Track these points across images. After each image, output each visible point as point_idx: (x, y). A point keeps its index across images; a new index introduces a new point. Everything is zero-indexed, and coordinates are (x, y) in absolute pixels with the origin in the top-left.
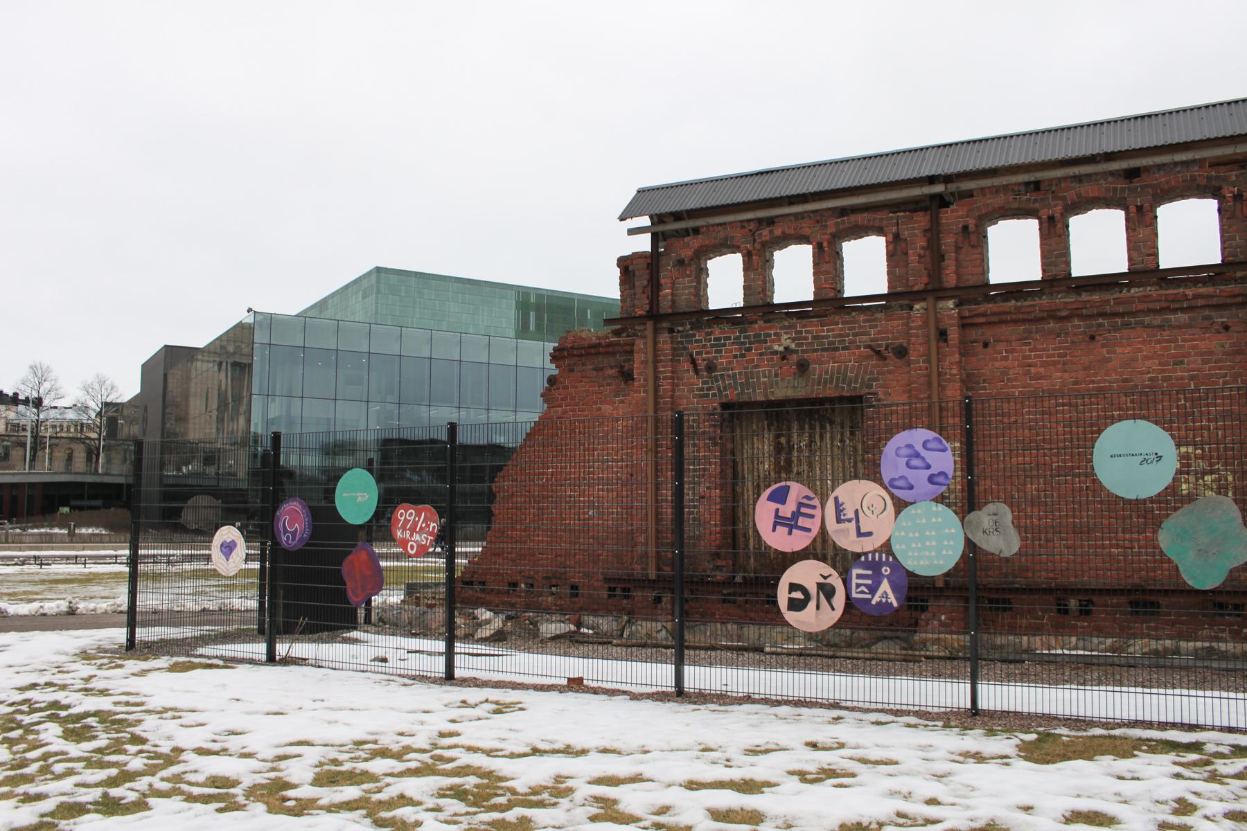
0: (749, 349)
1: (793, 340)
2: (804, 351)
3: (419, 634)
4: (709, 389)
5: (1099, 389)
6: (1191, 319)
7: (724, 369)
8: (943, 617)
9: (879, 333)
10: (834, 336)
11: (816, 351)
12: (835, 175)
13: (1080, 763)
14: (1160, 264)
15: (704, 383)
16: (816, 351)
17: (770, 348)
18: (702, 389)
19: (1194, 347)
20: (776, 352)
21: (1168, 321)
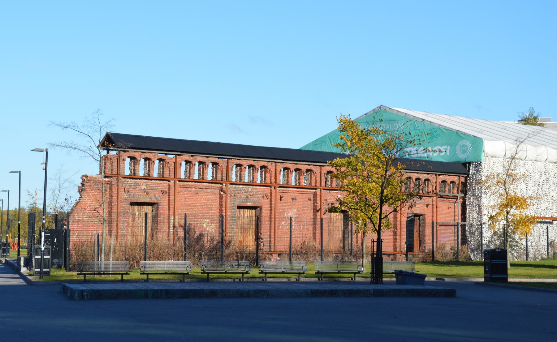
0: (136, 187)
1: (146, 186)
2: (148, 190)
3: (65, 242)
4: (128, 197)
5: (196, 205)
6: (211, 191)
7: (131, 192)
8: (50, 240)
9: (162, 187)
10: (154, 186)
11: (150, 190)
12: (330, 146)
13: (472, 266)
14: (125, 172)
15: (127, 195)
16: (150, 190)
17: (141, 187)
18: (126, 197)
19: (211, 197)
20: (142, 189)
21: (207, 191)
